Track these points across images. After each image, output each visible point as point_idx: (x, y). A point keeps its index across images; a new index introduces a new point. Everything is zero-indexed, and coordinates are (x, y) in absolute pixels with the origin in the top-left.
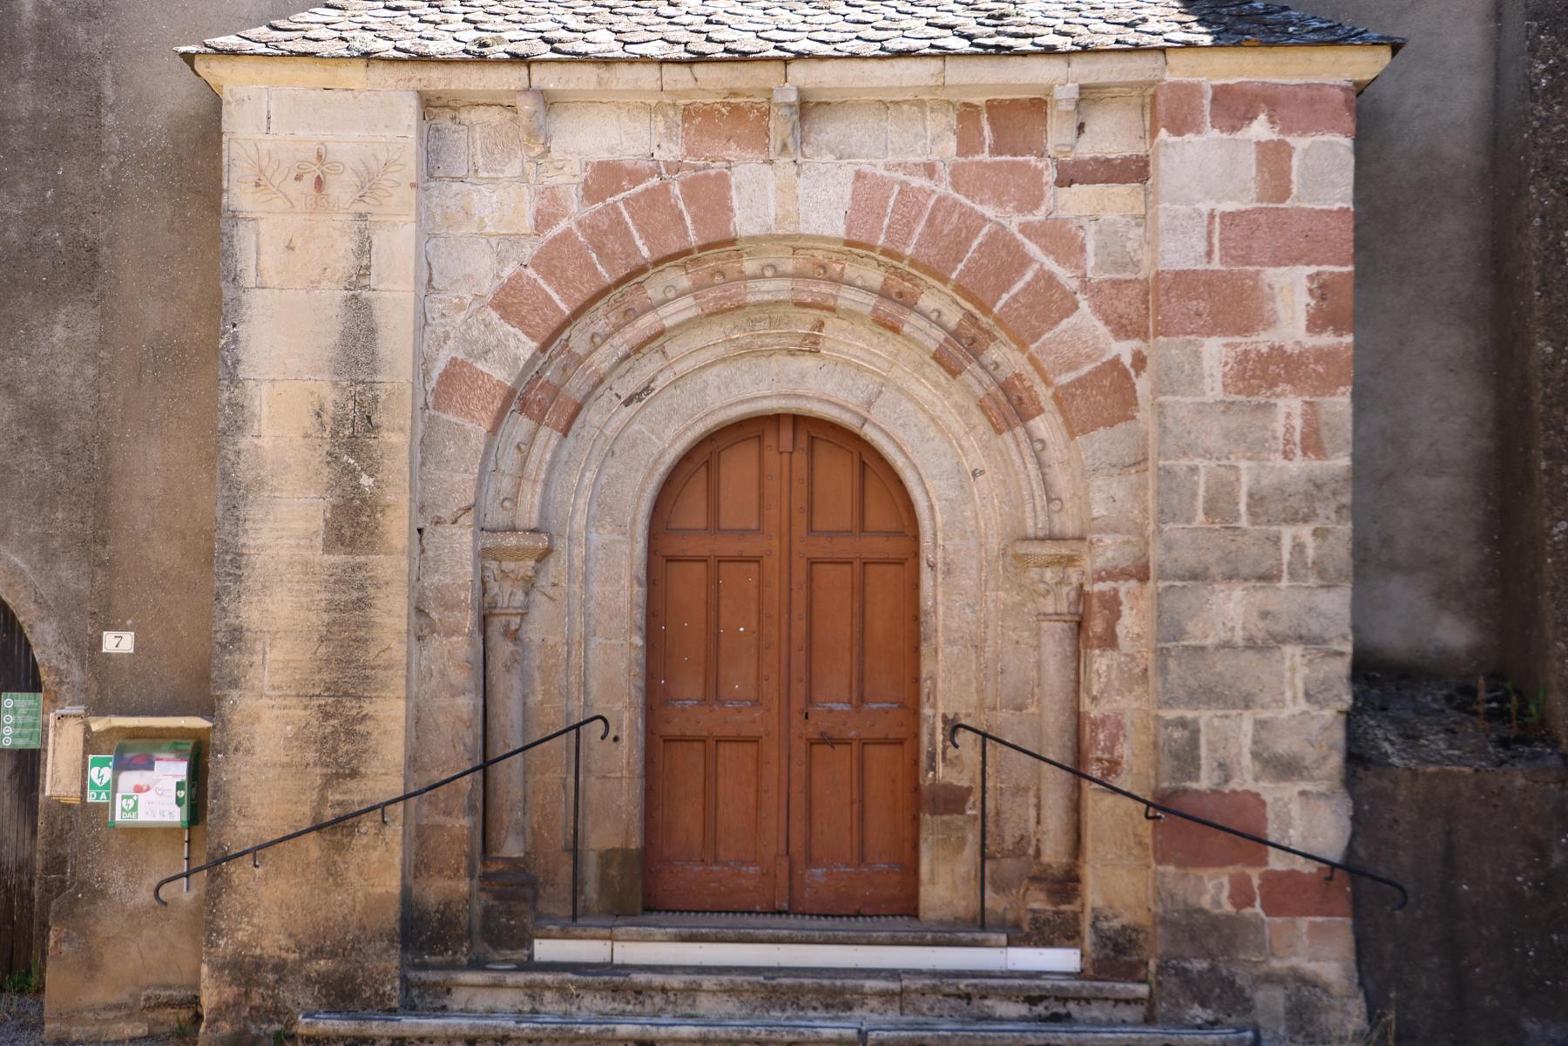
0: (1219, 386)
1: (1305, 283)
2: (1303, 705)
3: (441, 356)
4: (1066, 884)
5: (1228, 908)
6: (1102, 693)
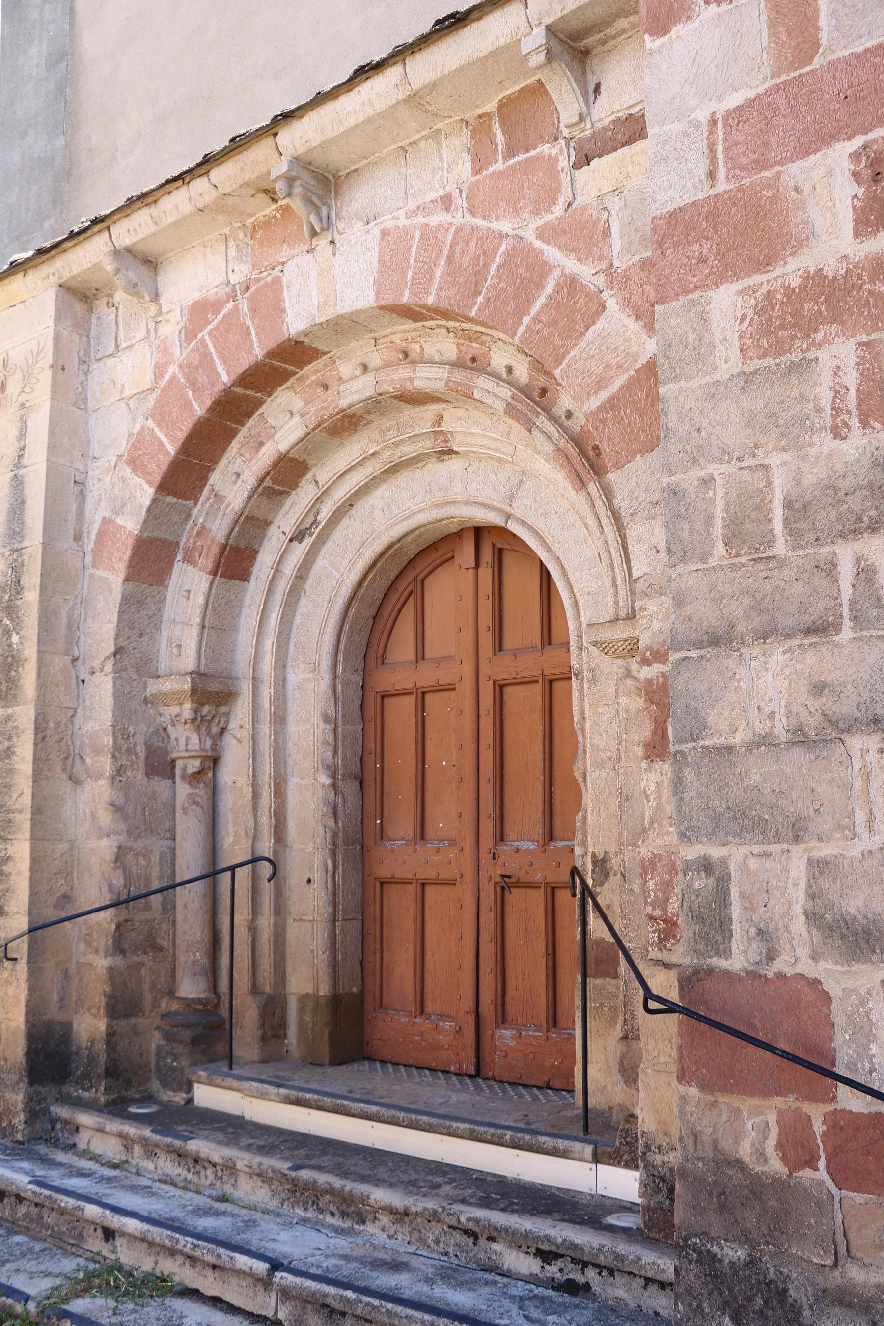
0: (735, 353)
1: (847, 165)
5: (776, 1166)
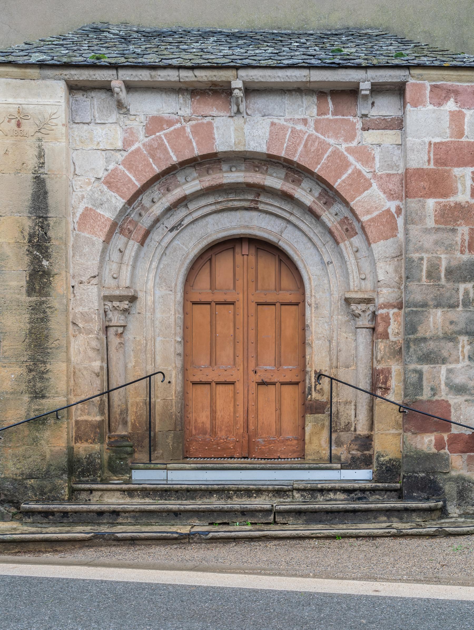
2: (467, 362)
3: (80, 206)
4: (366, 442)
5: (434, 450)
6: (382, 358)
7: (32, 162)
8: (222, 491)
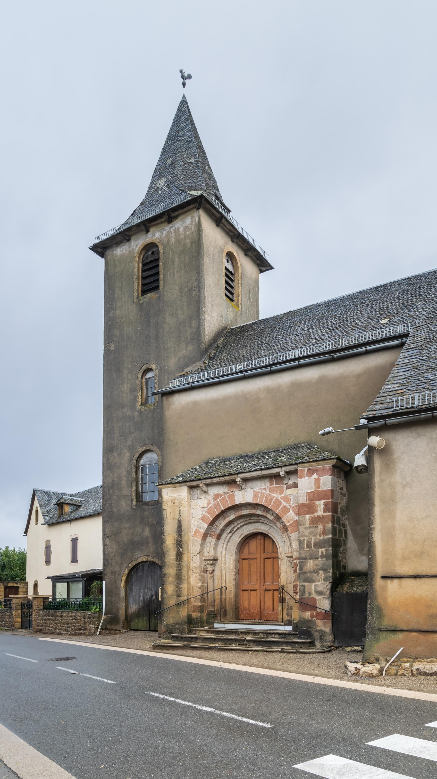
2: (323, 582)
5: (310, 618)
7: (177, 515)
8: (236, 632)
